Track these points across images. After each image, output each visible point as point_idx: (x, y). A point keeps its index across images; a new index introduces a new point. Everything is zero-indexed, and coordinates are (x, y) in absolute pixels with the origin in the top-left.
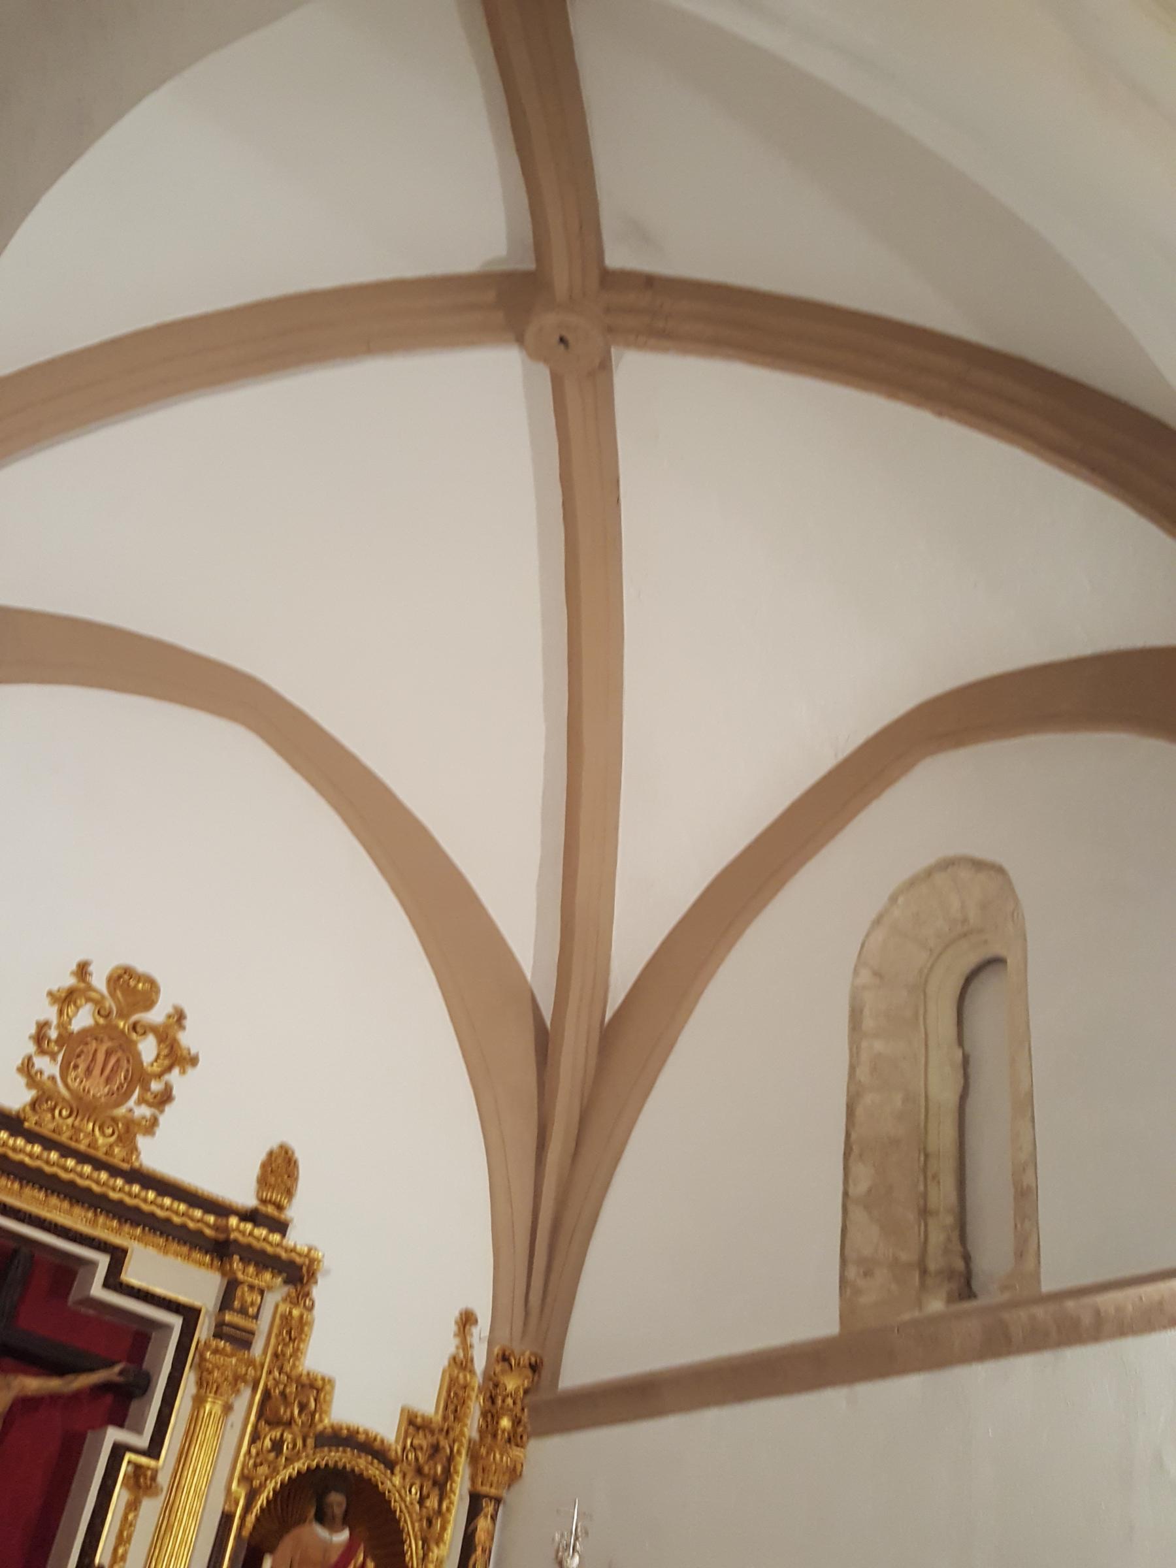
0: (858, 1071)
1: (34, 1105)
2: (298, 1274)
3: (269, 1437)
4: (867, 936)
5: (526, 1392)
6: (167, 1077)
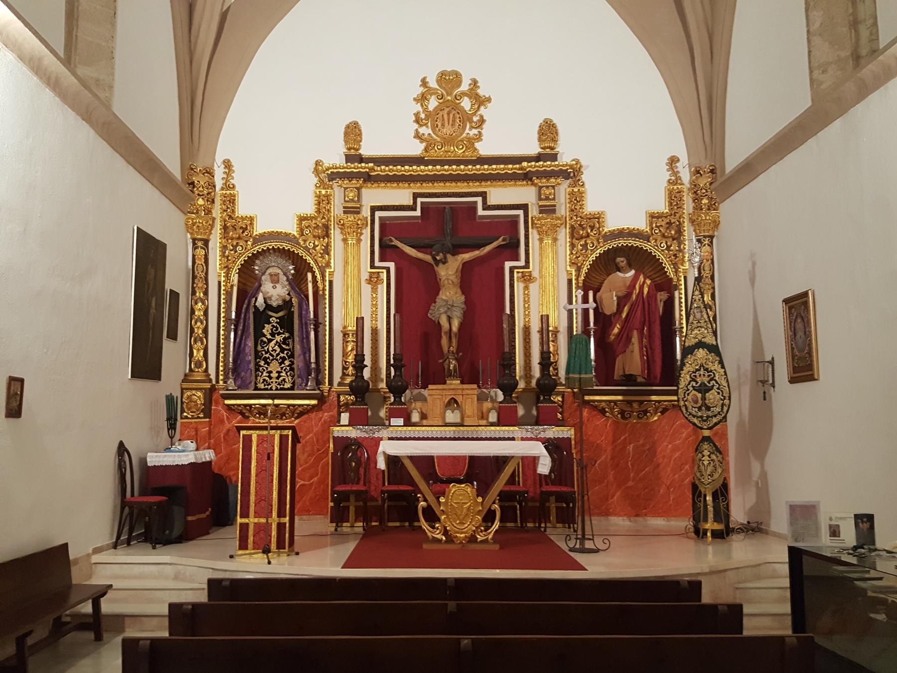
1: (426, 150)
2: (572, 174)
3: (579, 245)
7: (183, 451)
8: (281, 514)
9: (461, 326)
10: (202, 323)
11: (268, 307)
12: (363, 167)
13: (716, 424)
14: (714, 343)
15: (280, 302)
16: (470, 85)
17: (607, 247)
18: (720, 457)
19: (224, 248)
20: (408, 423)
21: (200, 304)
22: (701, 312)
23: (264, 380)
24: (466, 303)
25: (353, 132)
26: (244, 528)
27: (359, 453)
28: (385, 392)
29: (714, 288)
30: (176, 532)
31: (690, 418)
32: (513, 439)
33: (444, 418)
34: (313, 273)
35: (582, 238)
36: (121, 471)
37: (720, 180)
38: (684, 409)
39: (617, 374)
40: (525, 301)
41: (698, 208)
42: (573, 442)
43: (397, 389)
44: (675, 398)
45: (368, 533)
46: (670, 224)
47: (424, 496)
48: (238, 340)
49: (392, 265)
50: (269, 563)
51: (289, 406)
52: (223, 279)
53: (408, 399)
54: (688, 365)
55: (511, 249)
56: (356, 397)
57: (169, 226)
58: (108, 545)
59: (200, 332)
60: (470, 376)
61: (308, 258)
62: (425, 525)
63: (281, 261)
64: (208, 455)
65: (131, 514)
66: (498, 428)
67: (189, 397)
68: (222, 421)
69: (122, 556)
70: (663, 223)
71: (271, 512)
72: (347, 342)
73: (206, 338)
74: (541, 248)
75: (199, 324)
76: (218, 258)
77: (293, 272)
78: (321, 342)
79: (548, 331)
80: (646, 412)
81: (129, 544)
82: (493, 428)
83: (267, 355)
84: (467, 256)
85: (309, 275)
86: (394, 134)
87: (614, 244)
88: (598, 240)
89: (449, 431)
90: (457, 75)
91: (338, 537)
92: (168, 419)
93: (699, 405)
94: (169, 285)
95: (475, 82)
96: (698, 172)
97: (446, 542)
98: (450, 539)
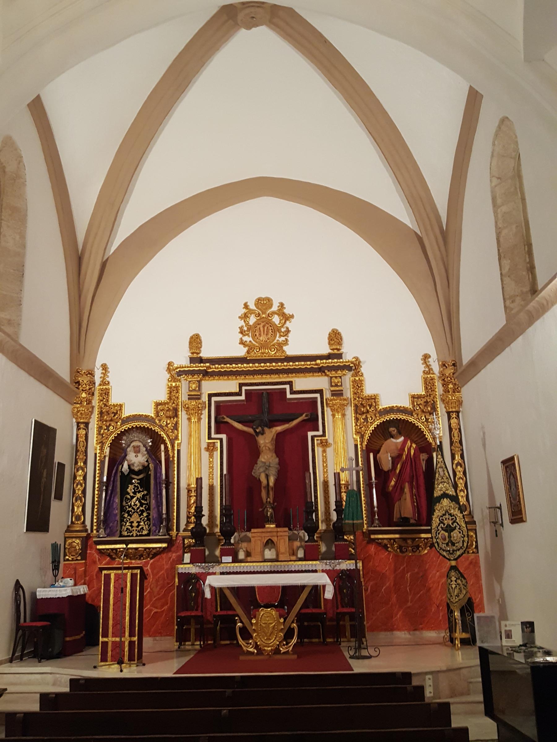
0: (498, 223)
1: (248, 352)
2: (354, 367)
3: (362, 418)
4: (491, 165)
5: (453, 374)
6: (285, 326)
7: (63, 587)
8: (131, 634)
9: (276, 481)
10: (81, 486)
11: (131, 471)
12: (202, 366)
13: (459, 556)
14: (454, 494)
15: (141, 468)
16: (278, 307)
17: (382, 419)
18: (464, 581)
19: (100, 428)
20: (236, 560)
21: (80, 471)
22: (444, 471)
23: (127, 529)
24: (279, 464)
25: (195, 341)
26: (105, 644)
27: (198, 586)
28: (219, 536)
29: (462, 450)
30: (57, 650)
31: (441, 551)
32: (316, 571)
33: (263, 555)
34: (166, 445)
35: (363, 413)
36: (17, 602)
37: (459, 371)
38: (436, 545)
39: (396, 516)
40: (323, 461)
41: (446, 391)
42: (361, 573)
43: (227, 533)
44: (429, 536)
45: (203, 649)
46: (427, 402)
47: (240, 619)
48: (108, 498)
49: (224, 437)
50: (121, 671)
51: (145, 549)
52: (98, 451)
53: (237, 539)
54: (437, 511)
55: (312, 422)
56: (196, 541)
57: (59, 415)
58: (6, 660)
59: (80, 492)
60: (284, 521)
61: (162, 433)
62: (241, 642)
63: (143, 437)
64: (82, 589)
65: (24, 635)
66: (304, 563)
67: (70, 544)
68: (94, 562)
69: (16, 668)
70: (422, 402)
71: (125, 633)
72: (191, 496)
73: (85, 497)
74: (334, 421)
75: (79, 486)
76: (95, 436)
77: (150, 444)
78: (171, 497)
79: (340, 484)
80: (418, 547)
81: (21, 660)
82: (300, 563)
83: (130, 509)
84: (279, 429)
85: (162, 447)
86: (225, 342)
87: (387, 418)
88: (375, 415)
89: (267, 566)
90: (269, 300)
91: (180, 651)
92: (53, 562)
93: (447, 541)
94: (58, 459)
95: (282, 305)
96: (444, 365)
97: (257, 654)
98: (260, 651)
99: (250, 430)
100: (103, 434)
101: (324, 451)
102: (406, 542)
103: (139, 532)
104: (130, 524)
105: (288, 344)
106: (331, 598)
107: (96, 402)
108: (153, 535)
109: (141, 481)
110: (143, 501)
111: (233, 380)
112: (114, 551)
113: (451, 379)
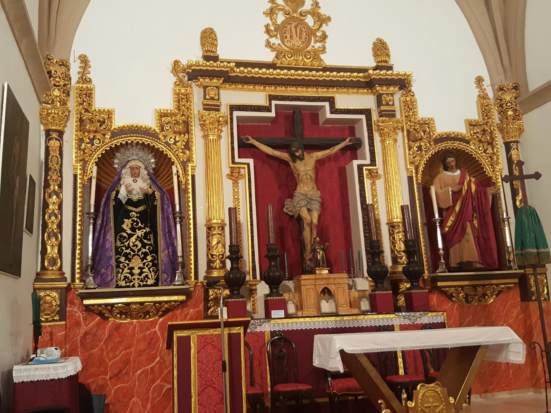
6: (321, 29)
10: (56, 217)
33: (319, 308)
49: (251, 161)
51: (155, 303)
68: (78, 324)
73: (61, 233)
83: (128, 251)
86: (247, 42)
88: (429, 143)
99: (284, 155)
100: (85, 149)
101: (373, 184)
102: (476, 290)
103: (142, 281)
104: (129, 271)
105: (326, 52)
106: (523, 363)
107: (72, 103)
108: (162, 285)
109: (142, 216)
110: (145, 241)
111: (260, 91)
112: (109, 307)
113: (512, 105)
